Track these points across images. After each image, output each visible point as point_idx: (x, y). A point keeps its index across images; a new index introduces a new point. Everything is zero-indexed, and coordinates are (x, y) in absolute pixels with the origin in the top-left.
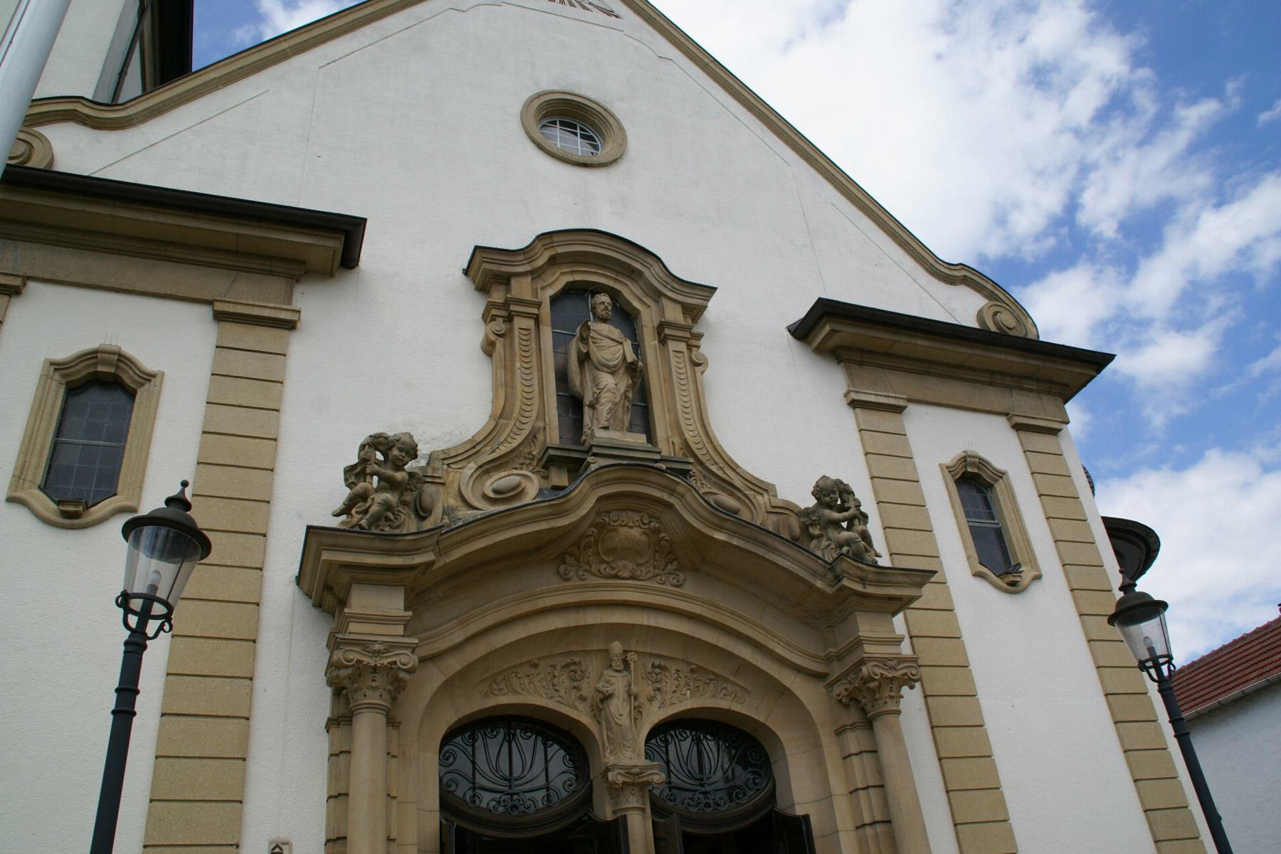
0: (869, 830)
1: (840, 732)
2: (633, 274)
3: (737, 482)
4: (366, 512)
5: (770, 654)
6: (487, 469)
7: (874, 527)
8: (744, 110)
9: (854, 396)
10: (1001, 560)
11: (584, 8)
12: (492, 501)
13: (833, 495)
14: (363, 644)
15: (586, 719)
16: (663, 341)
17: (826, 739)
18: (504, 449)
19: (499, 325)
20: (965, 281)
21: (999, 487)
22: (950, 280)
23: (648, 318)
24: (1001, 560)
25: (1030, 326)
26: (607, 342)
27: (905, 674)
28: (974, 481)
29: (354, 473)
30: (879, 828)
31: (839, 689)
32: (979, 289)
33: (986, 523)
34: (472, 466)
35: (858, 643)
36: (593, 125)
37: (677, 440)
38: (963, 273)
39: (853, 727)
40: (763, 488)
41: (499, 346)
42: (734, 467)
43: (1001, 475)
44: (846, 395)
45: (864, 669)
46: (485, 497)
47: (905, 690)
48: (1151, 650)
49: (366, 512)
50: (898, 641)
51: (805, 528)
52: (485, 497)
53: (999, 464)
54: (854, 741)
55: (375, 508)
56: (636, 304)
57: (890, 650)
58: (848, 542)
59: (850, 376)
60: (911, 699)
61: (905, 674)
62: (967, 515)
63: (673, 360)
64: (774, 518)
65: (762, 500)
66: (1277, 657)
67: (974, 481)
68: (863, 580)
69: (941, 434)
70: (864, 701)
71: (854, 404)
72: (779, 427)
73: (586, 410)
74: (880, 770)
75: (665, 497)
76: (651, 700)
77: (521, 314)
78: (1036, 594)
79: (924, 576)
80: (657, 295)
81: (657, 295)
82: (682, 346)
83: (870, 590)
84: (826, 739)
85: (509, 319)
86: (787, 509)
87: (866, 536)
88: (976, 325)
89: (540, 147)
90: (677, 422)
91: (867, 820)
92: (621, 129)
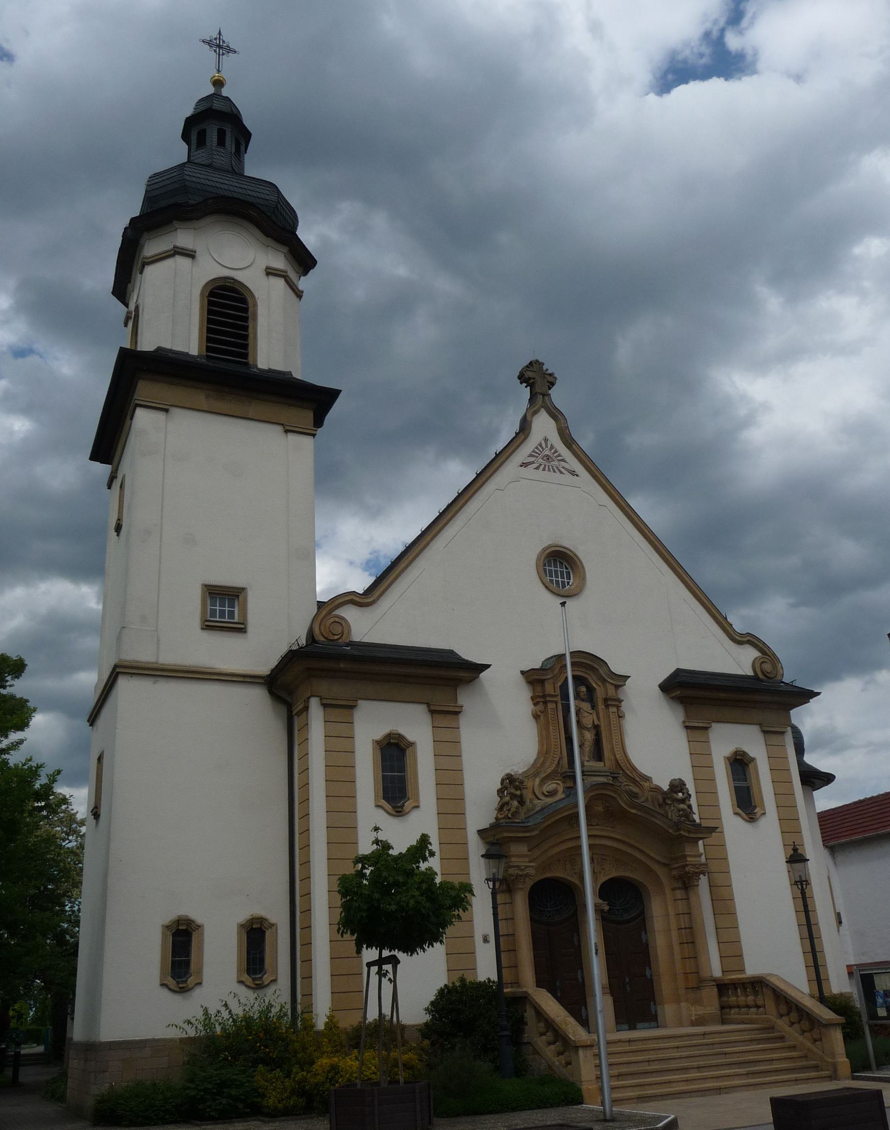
0: (683, 931)
1: (673, 889)
2: (593, 669)
4: (509, 810)
5: (648, 856)
6: (543, 781)
7: (693, 801)
8: (642, 538)
9: (687, 724)
10: (747, 804)
11: (561, 472)
12: (546, 796)
13: (678, 786)
14: (517, 867)
15: (577, 882)
16: (607, 706)
17: (668, 891)
18: (549, 771)
19: (541, 707)
20: (749, 642)
21: (751, 766)
22: (740, 643)
23: (600, 693)
24: (747, 804)
26: (586, 714)
27: (703, 869)
28: (740, 764)
29: (500, 792)
31: (675, 873)
32: (755, 646)
33: (742, 784)
34: (537, 780)
37: (613, 758)
38: (748, 638)
39: (679, 888)
40: (648, 779)
41: (542, 717)
42: (634, 769)
43: (753, 760)
44: (684, 722)
45: (687, 869)
46: (543, 794)
47: (702, 876)
49: (509, 810)
50: (700, 855)
51: (664, 799)
53: (752, 754)
54: (679, 894)
55: (513, 810)
56: (594, 685)
57: (697, 859)
58: (683, 810)
59: (686, 711)
60: (703, 881)
61: (703, 869)
62: (734, 780)
63: (612, 717)
64: (651, 793)
65: (646, 784)
66: (887, 814)
67: (740, 764)
68: (689, 832)
69: (728, 738)
70: (686, 882)
71: (687, 727)
72: (656, 745)
74: (689, 908)
75: (613, 795)
76: (600, 873)
77: (550, 701)
78: (763, 822)
79: (713, 829)
80: (604, 681)
81: (604, 681)
82: (615, 709)
83: (691, 835)
84: (668, 891)
85: (545, 703)
86: (658, 789)
87: (690, 807)
89: (547, 587)
90: (613, 749)
92: (583, 568)
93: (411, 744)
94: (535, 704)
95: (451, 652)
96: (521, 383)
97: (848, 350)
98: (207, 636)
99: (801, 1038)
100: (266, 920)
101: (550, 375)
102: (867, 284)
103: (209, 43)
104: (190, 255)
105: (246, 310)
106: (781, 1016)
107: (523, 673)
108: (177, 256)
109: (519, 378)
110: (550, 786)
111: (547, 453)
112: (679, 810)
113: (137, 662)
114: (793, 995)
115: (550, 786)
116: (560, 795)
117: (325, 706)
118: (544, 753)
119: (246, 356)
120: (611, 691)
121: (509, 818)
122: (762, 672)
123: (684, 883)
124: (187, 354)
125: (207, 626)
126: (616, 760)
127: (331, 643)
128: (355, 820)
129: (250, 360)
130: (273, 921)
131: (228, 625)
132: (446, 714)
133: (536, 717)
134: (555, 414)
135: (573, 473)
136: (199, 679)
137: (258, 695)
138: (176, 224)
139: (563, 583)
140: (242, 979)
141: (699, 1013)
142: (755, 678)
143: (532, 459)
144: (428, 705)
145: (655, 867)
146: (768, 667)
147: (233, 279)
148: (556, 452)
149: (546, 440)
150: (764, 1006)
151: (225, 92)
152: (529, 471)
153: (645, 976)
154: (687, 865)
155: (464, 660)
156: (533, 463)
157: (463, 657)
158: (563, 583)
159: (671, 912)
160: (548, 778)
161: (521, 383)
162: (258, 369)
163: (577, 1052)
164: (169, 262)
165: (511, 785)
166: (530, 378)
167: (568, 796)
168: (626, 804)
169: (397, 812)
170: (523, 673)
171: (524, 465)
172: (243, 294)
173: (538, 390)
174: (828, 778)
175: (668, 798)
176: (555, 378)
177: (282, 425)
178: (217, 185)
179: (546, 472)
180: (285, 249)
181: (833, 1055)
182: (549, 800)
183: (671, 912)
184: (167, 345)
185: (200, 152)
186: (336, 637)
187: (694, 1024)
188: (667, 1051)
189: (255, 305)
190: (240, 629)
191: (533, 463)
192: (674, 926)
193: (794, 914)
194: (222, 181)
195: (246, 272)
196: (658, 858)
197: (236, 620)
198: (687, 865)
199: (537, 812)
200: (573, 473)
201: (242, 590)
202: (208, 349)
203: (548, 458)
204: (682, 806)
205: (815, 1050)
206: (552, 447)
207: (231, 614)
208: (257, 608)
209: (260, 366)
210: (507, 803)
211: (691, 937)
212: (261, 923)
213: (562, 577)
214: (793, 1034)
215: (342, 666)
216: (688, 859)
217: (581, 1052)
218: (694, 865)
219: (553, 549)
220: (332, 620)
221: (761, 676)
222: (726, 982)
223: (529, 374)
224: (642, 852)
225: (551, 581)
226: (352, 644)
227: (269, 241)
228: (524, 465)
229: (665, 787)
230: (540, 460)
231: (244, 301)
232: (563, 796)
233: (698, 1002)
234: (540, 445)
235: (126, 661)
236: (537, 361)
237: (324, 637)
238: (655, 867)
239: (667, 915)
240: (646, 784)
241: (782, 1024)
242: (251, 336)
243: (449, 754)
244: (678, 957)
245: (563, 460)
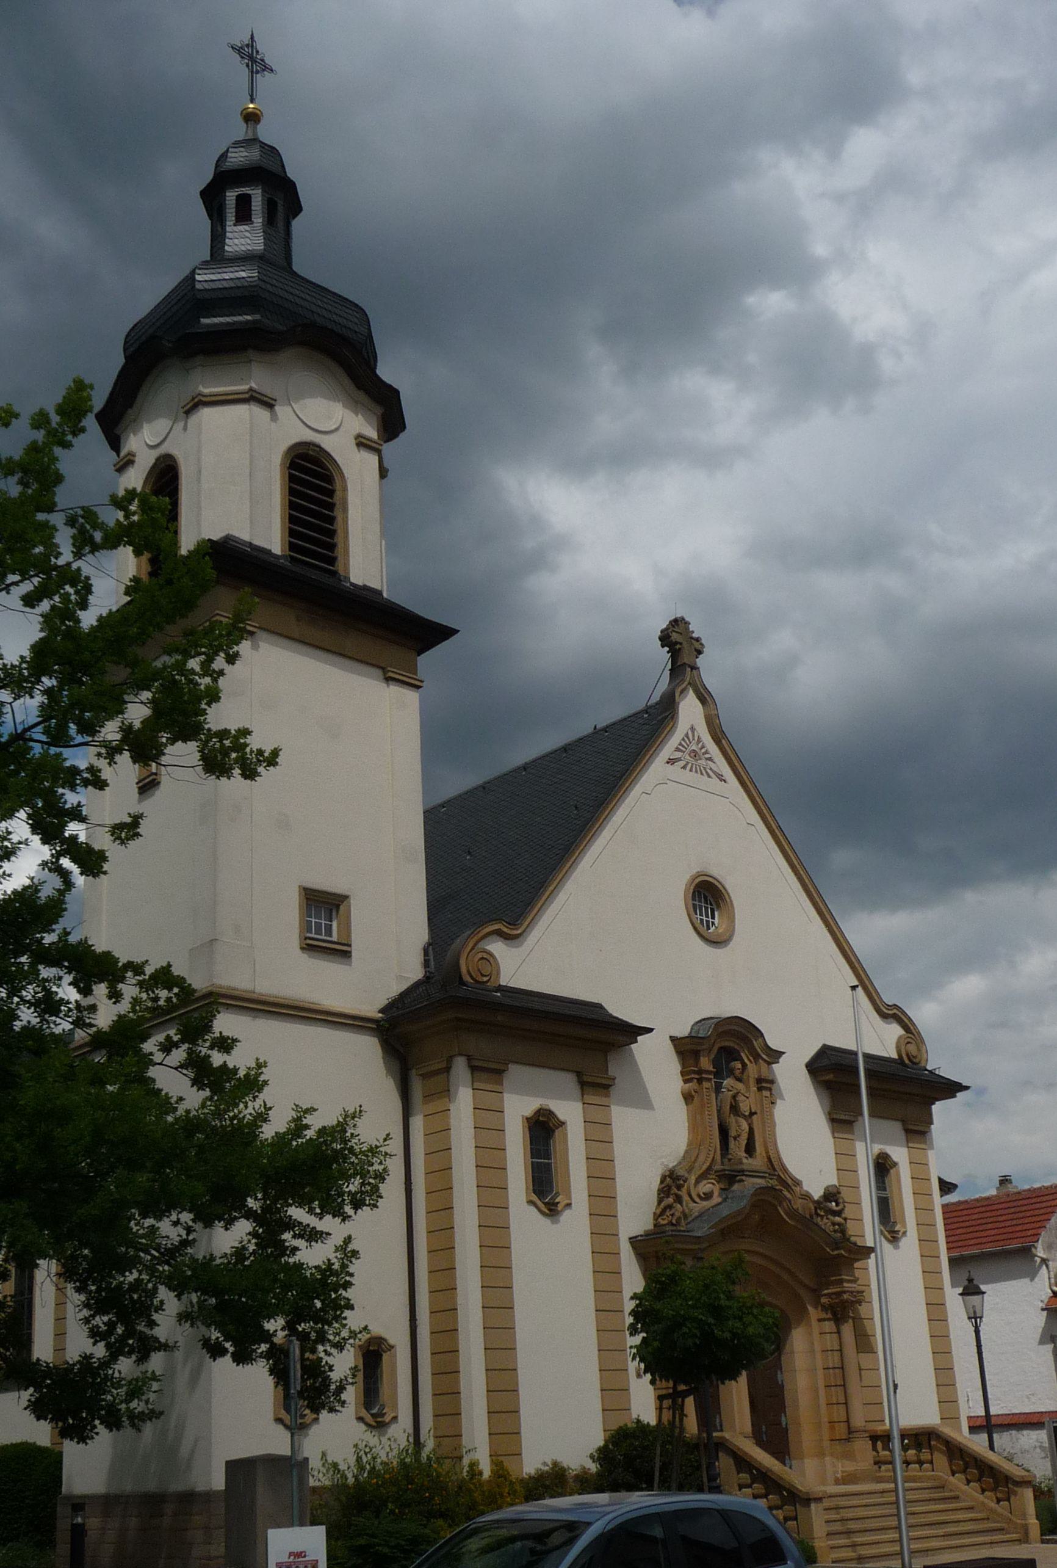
3: (790, 1182)
11: (709, 776)
16: (760, 1089)
17: (814, 1323)
18: (705, 1167)
22: (884, 1016)
25: (924, 1051)
28: (883, 1167)
30: (837, 1371)
33: (883, 1194)
35: (841, 1281)
36: (718, 906)
38: (895, 1011)
39: (829, 1320)
40: (798, 1183)
42: (785, 1170)
43: (895, 1164)
46: (699, 1196)
48: (975, 1312)
49: (672, 1215)
52: (699, 1196)
54: (829, 1326)
55: (677, 1214)
58: (839, 1224)
67: (883, 1167)
72: (804, 1142)
73: (731, 1140)
88: (895, 1056)
89: (695, 929)
91: (831, 1366)
93: (562, 1124)
94: (686, 1081)
95: (599, 1006)
96: (663, 646)
97: (712, 459)
98: (304, 958)
99: (981, 1498)
100: (385, 1340)
101: (698, 640)
102: (752, 358)
103: (238, 50)
104: (268, 404)
105: (331, 493)
106: (953, 1473)
107: (673, 1039)
108: (252, 403)
109: (661, 639)
110: (705, 1187)
111: (694, 748)
112: (834, 1224)
113: (235, 989)
114: (975, 1448)
115: (705, 1187)
116: (716, 1199)
117: (473, 1069)
118: (694, 1145)
119: (332, 561)
120: (765, 1073)
121: (673, 1224)
122: (907, 1055)
123: (834, 1314)
124: (268, 552)
125: (308, 945)
126: (769, 1159)
127: (478, 986)
128: (507, 1218)
129: (340, 567)
130: (392, 1342)
131: (324, 945)
132: (595, 1085)
133: (688, 1097)
134: (704, 697)
135: (722, 779)
136: (346, 1024)
137: (368, 1047)
138: (251, 353)
139: (708, 922)
140: (361, 1415)
141: (847, 1469)
142: (900, 1061)
143: (678, 755)
144: (579, 1074)
145: (802, 1292)
146: (912, 1049)
147: (319, 447)
148: (703, 747)
149: (693, 729)
150: (931, 1462)
151: (266, 133)
152: (675, 770)
153: (780, 1424)
154: (845, 1292)
155: (611, 1016)
156: (679, 760)
157: (615, 1014)
158: (708, 922)
159: (818, 1348)
160: (703, 1176)
161: (663, 646)
162: (352, 584)
163: (809, 1506)
164: (242, 410)
165: (671, 1184)
166: (677, 643)
167: (725, 1200)
168: (786, 1214)
169: (550, 1210)
170: (673, 1039)
171: (671, 761)
172: (328, 469)
173: (686, 661)
174: (955, 1186)
175: (821, 1209)
176: (702, 645)
177: (383, 668)
178: (298, 301)
179: (693, 774)
180: (380, 410)
181: (1024, 1516)
182: (706, 1204)
183: (818, 1348)
184: (244, 534)
185: (241, 228)
186: (485, 979)
187: (837, 1482)
188: (856, 1510)
189: (345, 489)
190: (341, 952)
191: (679, 760)
192: (819, 1364)
193: (931, 1355)
194: (302, 295)
195: (332, 436)
196: (807, 1282)
197: (335, 938)
198: (845, 1292)
199: (697, 1217)
200: (722, 779)
201: (344, 898)
202: (292, 547)
203: (695, 754)
204: (837, 1219)
205: (999, 1510)
206: (699, 741)
207: (329, 932)
208: (364, 923)
209: (353, 580)
210: (670, 1207)
211: (839, 1380)
212: (379, 1345)
213: (707, 916)
214: (971, 1492)
215: (499, 1018)
216: (845, 1284)
217: (813, 1506)
218: (852, 1292)
219: (710, 879)
220: (480, 955)
221: (907, 1061)
222: (879, 1433)
223: (675, 637)
224: (789, 1271)
225: (702, 920)
226: (501, 988)
227: (361, 396)
228: (671, 761)
229: (817, 1193)
230: (688, 757)
231: (329, 479)
232: (720, 1200)
233: (848, 1456)
234: (687, 735)
235: (221, 987)
236: (683, 619)
237: (471, 976)
238: (802, 1292)
239: (812, 1351)
240: (797, 1189)
241: (957, 1481)
242: (340, 532)
243: (600, 1136)
244: (823, 1401)
245: (710, 759)
